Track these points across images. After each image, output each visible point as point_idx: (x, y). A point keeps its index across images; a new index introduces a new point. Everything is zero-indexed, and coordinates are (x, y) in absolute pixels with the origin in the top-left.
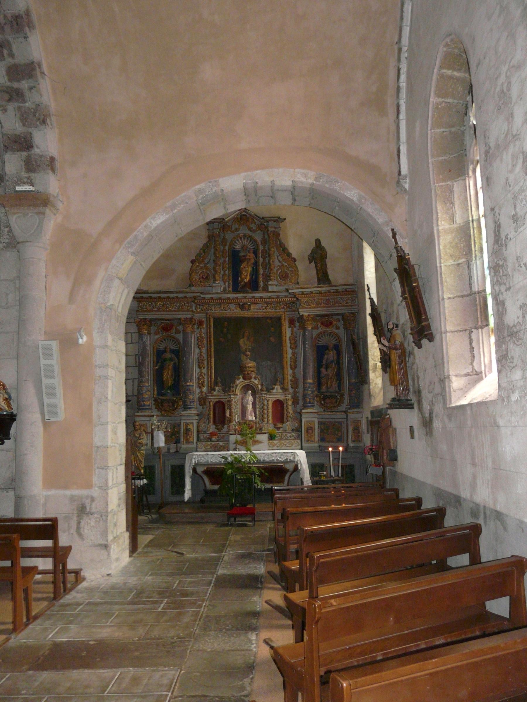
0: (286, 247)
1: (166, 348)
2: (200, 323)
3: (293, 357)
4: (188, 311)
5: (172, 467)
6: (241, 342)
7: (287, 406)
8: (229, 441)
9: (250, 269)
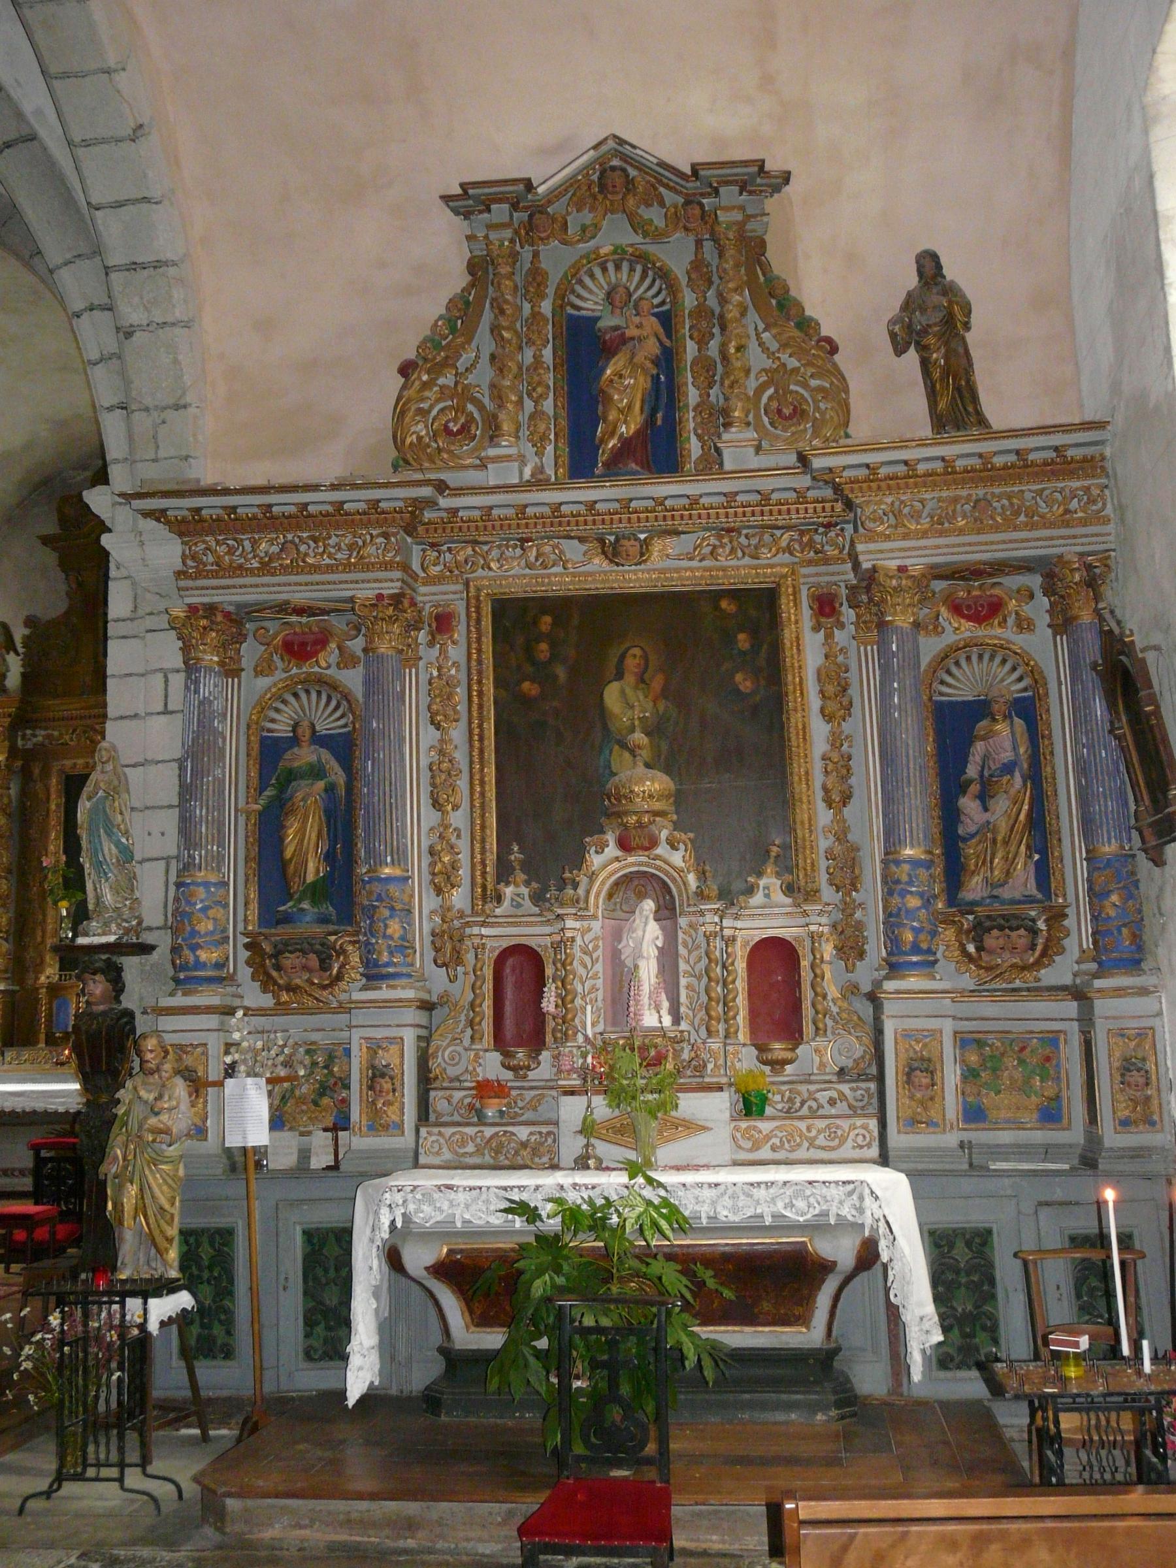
1: (295, 726)
2: (443, 623)
3: (835, 757)
4: (387, 566)
5: (308, 1234)
6: (612, 695)
7: (813, 966)
8: (557, 1124)
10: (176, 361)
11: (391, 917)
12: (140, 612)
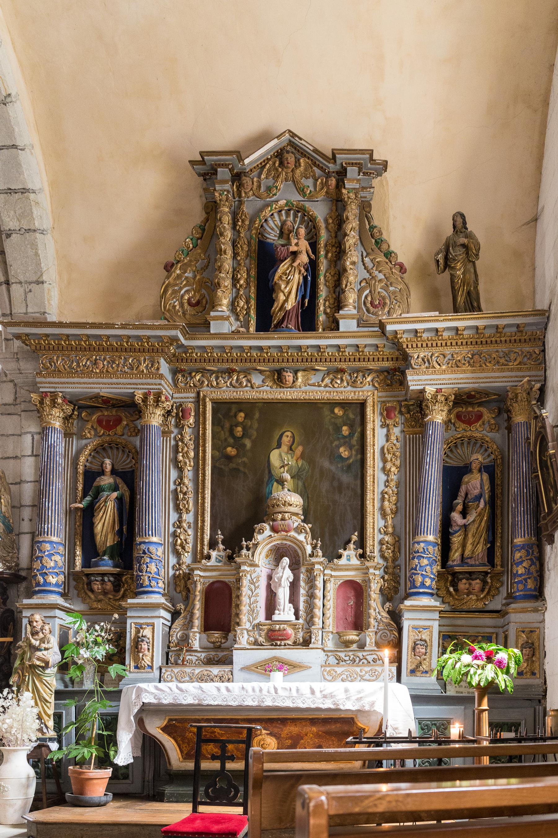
0: (385, 236)
6: (275, 457)
9: (296, 278)
10: (37, 254)
11: (150, 562)
12: (18, 401)
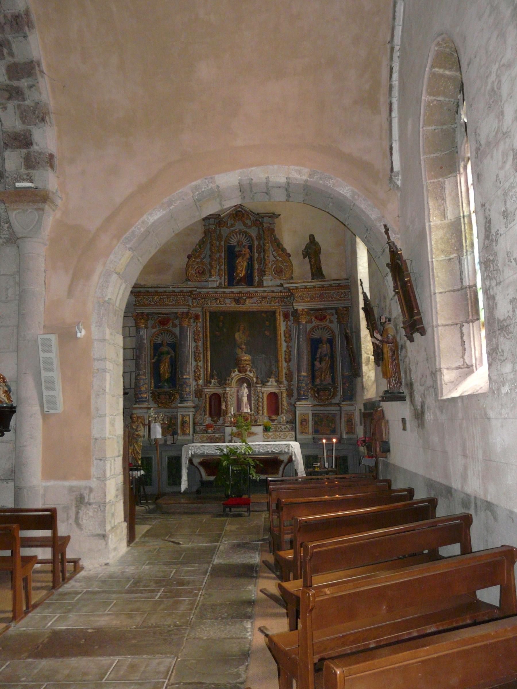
0: (281, 242)
1: (162, 342)
2: (197, 317)
3: (288, 351)
4: (185, 305)
5: (169, 458)
6: (237, 335)
7: (281, 399)
8: (224, 433)
9: (245, 264)
